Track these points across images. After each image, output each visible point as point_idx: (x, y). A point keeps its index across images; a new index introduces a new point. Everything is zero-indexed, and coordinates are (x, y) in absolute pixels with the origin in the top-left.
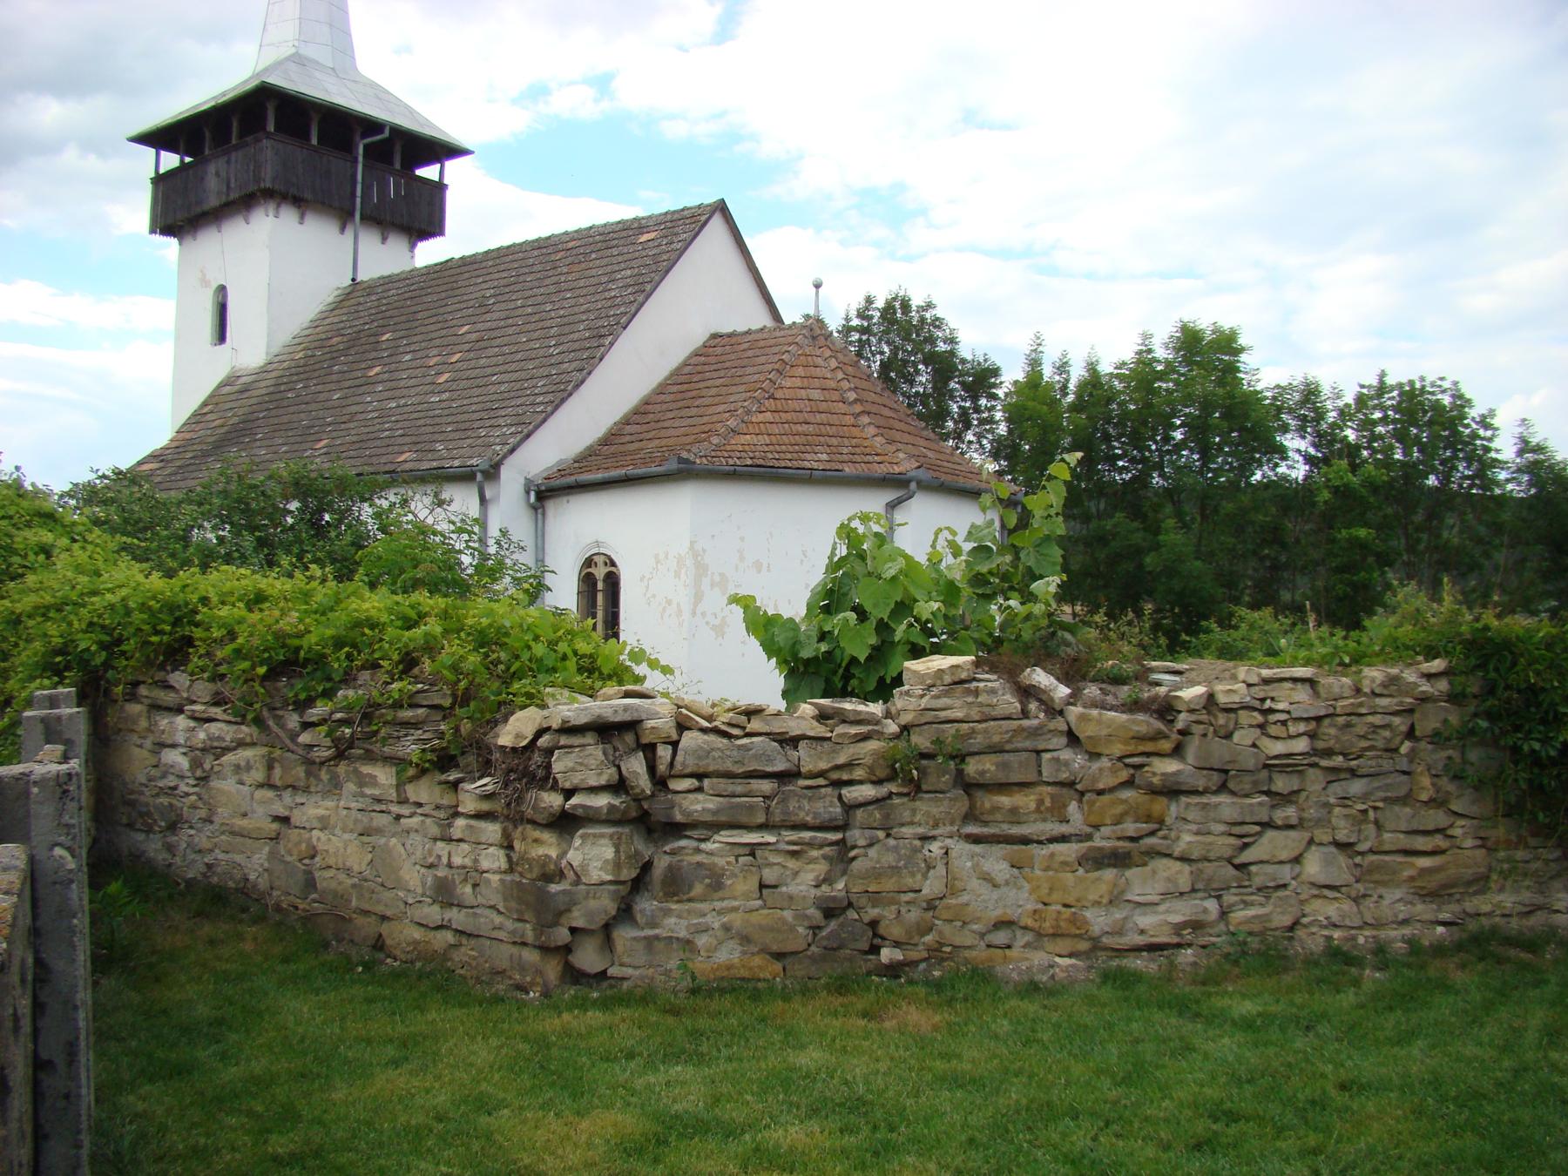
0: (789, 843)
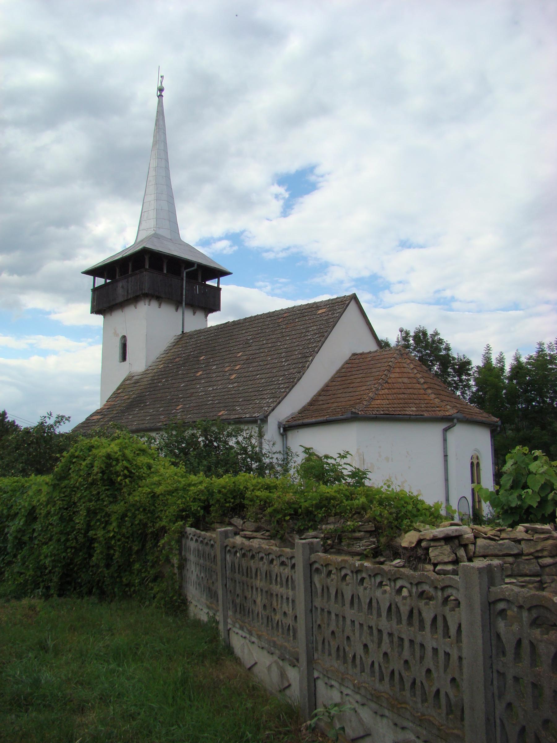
0: (522, 582)
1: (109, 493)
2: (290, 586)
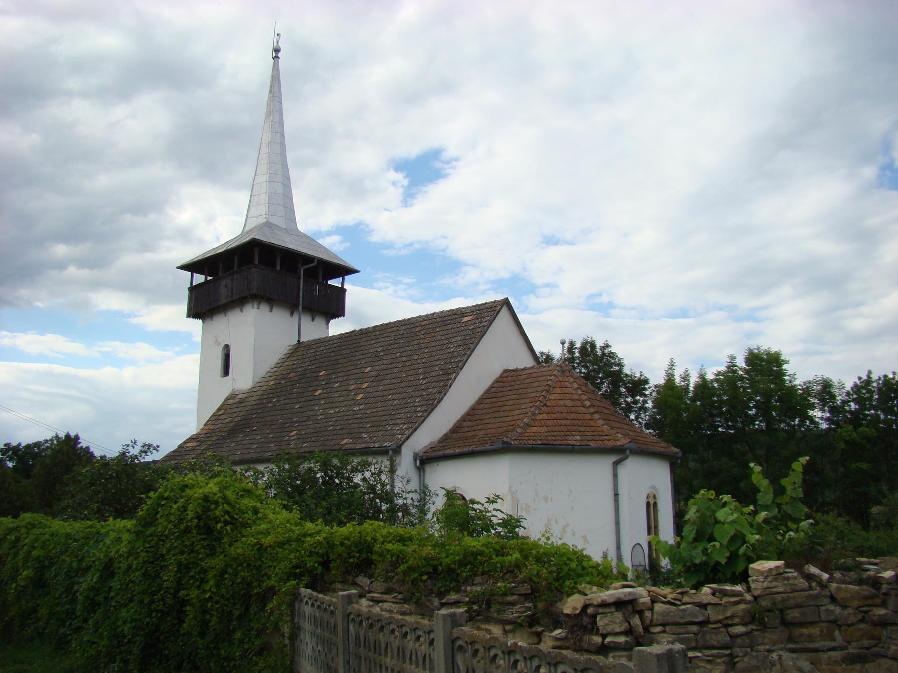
2: (427, 666)
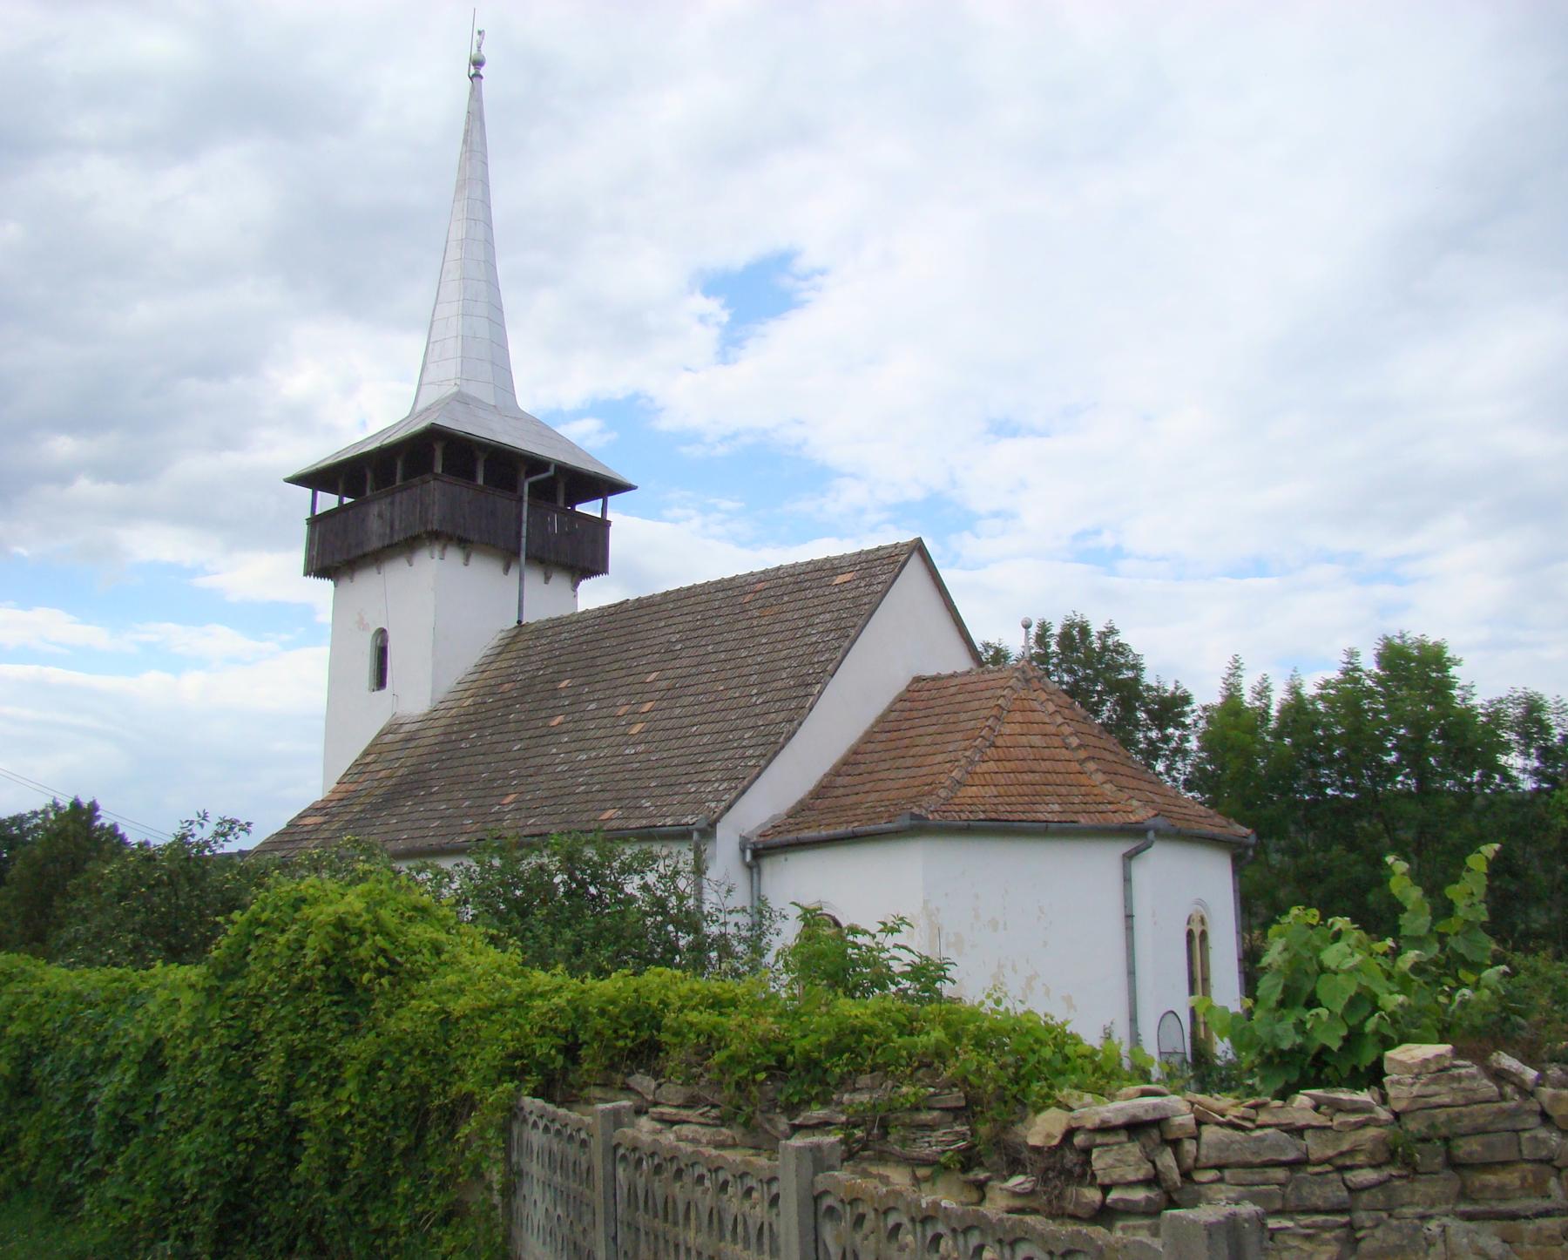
0: (1307, 1227)
1: (339, 1011)
2: (766, 1247)
